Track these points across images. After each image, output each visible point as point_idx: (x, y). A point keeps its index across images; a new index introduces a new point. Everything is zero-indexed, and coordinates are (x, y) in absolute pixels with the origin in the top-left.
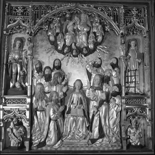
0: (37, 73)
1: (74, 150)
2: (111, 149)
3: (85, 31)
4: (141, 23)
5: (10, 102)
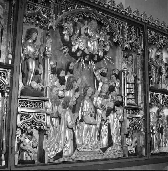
0: (52, 73)
1: (89, 159)
2: (117, 157)
3: (97, 38)
4: (45, 13)
5: (24, 105)
